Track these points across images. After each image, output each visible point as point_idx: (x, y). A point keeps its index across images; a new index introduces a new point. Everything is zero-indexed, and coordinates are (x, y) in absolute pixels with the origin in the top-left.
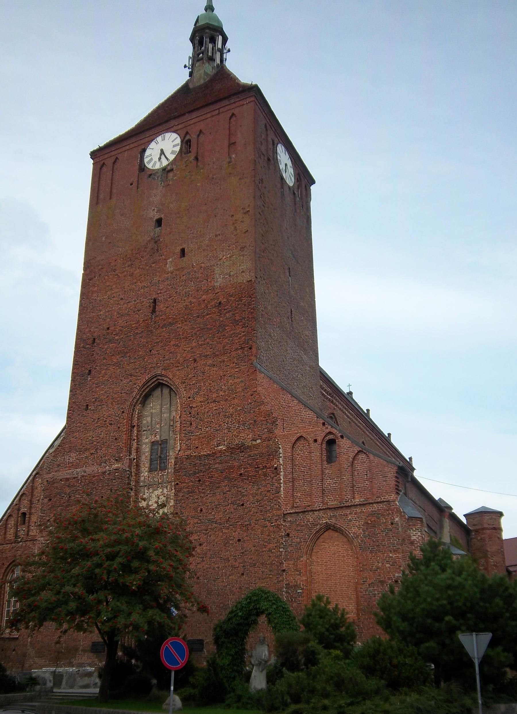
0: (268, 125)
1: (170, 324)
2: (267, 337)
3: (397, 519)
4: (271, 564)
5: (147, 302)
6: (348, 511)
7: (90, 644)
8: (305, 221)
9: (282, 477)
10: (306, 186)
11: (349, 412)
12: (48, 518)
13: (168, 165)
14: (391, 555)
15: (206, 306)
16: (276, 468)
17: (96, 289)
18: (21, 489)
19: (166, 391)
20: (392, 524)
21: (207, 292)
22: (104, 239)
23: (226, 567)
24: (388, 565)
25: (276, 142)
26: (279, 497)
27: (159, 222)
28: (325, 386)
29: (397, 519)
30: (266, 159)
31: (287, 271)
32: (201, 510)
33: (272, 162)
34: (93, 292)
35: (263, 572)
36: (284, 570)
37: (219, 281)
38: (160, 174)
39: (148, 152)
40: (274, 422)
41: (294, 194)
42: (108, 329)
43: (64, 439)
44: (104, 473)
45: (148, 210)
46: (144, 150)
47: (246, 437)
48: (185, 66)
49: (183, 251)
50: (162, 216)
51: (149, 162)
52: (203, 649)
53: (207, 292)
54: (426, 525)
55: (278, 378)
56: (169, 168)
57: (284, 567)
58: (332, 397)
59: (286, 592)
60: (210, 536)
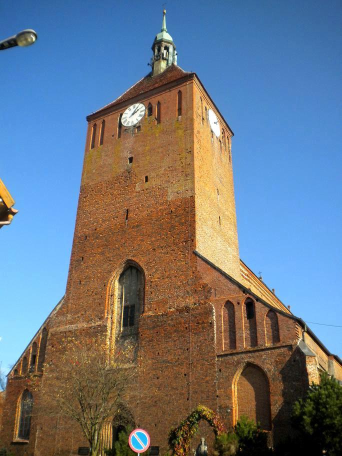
0: (202, 98)
1: (138, 226)
2: (203, 234)
3: (298, 358)
4: (208, 391)
5: (122, 212)
6: (263, 353)
7: (78, 448)
8: (228, 159)
9: (215, 330)
10: (228, 137)
11: (261, 288)
12: (51, 359)
13: (137, 123)
14: (294, 383)
15: (162, 214)
16: (211, 323)
17: (88, 204)
18: (33, 338)
19: (134, 271)
20: (294, 361)
21: (162, 204)
22: (94, 171)
23: (175, 394)
24: (292, 391)
25: (208, 109)
26: (213, 343)
27: (131, 160)
28: (243, 269)
29: (298, 358)
30: (201, 118)
31: (217, 191)
32: (158, 354)
33: (205, 120)
34: (86, 206)
35: (202, 398)
36: (217, 396)
37: (170, 198)
38: (132, 129)
39: (123, 116)
40: (209, 291)
41: (220, 141)
42: (96, 229)
43: (63, 304)
44: (90, 328)
45: (123, 152)
46: (121, 115)
47: (190, 301)
48: (149, 64)
49: (147, 178)
50: (133, 156)
51: (125, 122)
52: (158, 453)
53: (162, 204)
54: (318, 364)
55: (200, 112)
56: (138, 125)
57: (218, 393)
58: (249, 277)
59: (219, 412)
60: (164, 372)
